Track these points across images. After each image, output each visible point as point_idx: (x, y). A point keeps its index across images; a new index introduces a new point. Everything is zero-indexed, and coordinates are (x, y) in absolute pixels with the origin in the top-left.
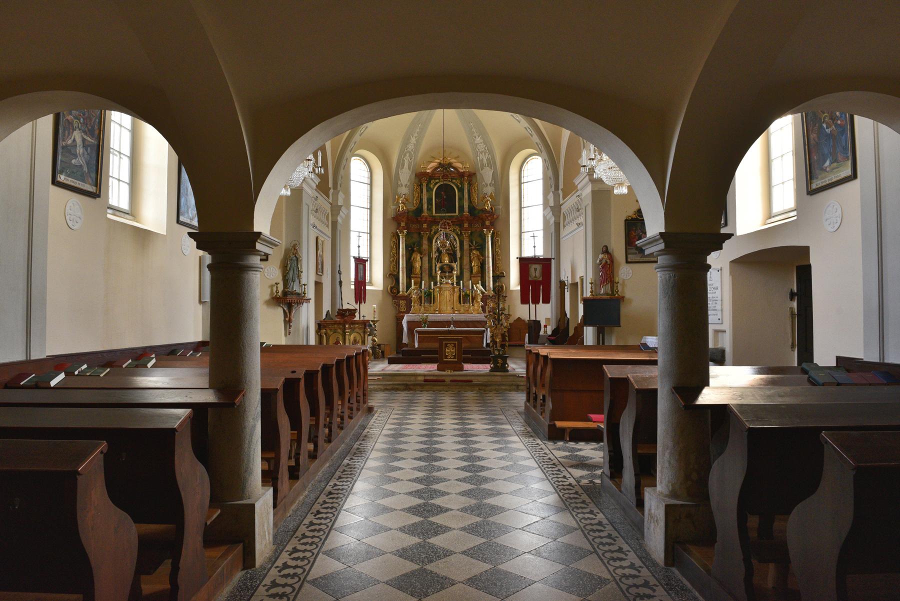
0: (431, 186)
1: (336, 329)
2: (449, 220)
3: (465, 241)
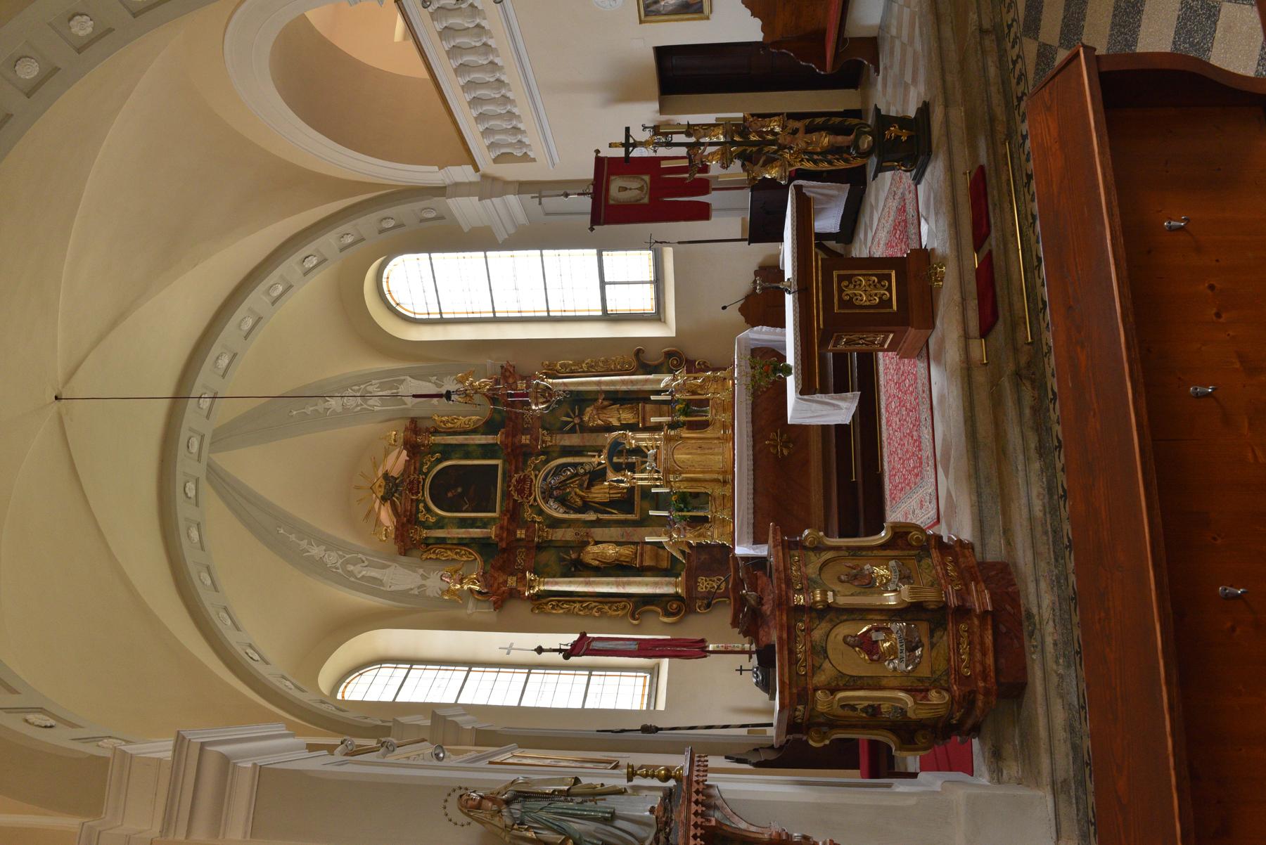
0: (432, 520)
1: (813, 647)
2: (511, 477)
3: (561, 444)
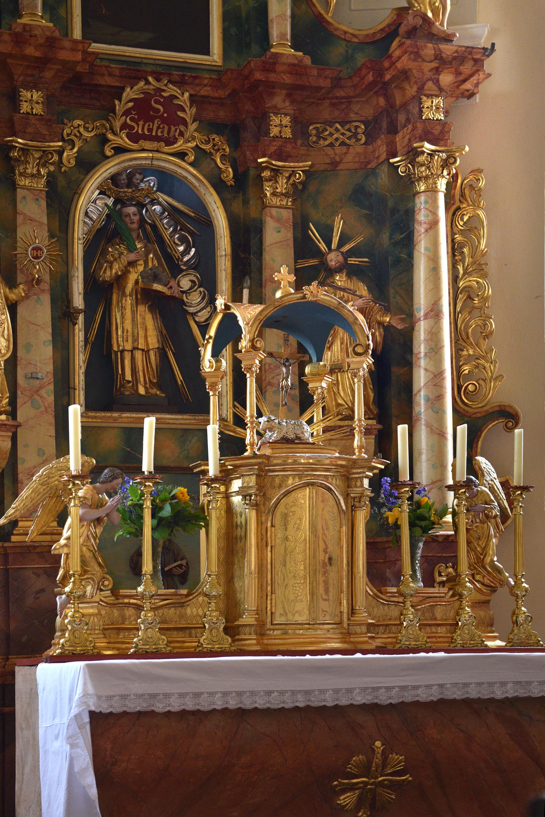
2: (181, 83)
